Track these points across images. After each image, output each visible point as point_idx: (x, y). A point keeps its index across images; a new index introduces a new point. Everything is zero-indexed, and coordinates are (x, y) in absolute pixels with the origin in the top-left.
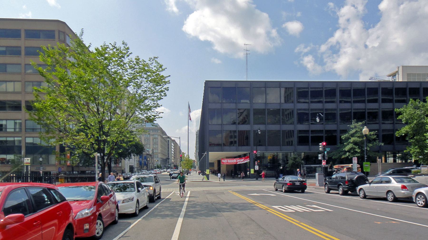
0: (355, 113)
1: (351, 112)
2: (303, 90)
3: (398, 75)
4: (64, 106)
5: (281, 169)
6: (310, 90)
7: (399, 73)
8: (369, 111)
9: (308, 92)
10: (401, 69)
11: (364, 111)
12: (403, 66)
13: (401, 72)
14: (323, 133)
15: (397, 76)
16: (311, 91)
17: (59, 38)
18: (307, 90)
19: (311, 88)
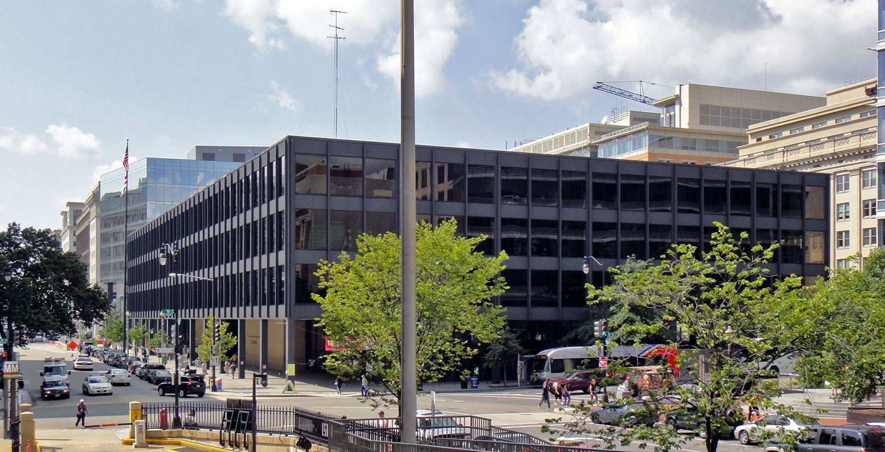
0: (524, 194)
1: (724, 189)
2: (740, 186)
3: (681, 105)
4: (778, 283)
5: (541, 333)
6: (649, 181)
7: (683, 101)
8: (653, 181)
9: (614, 186)
10: (686, 90)
11: (724, 185)
12: (692, 87)
13: (688, 100)
14: (596, 246)
15: (677, 107)
16: (622, 185)
17: (828, 95)
18: (613, 182)
19: (624, 176)
